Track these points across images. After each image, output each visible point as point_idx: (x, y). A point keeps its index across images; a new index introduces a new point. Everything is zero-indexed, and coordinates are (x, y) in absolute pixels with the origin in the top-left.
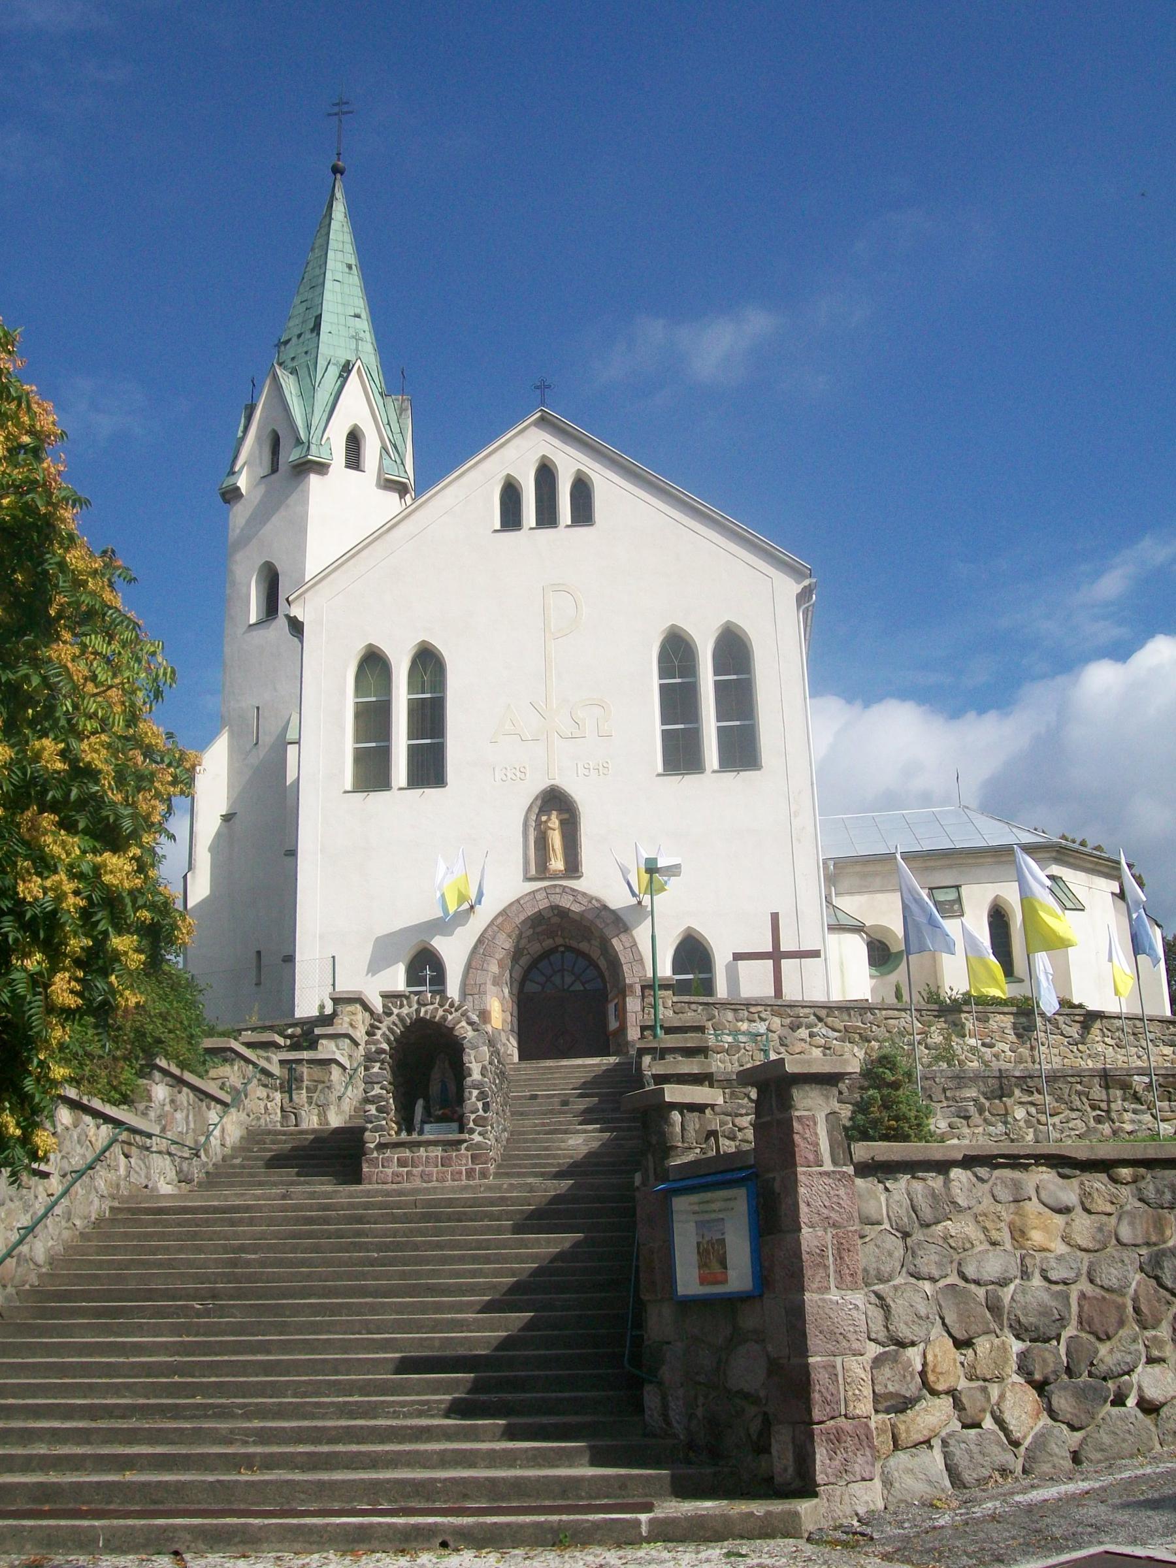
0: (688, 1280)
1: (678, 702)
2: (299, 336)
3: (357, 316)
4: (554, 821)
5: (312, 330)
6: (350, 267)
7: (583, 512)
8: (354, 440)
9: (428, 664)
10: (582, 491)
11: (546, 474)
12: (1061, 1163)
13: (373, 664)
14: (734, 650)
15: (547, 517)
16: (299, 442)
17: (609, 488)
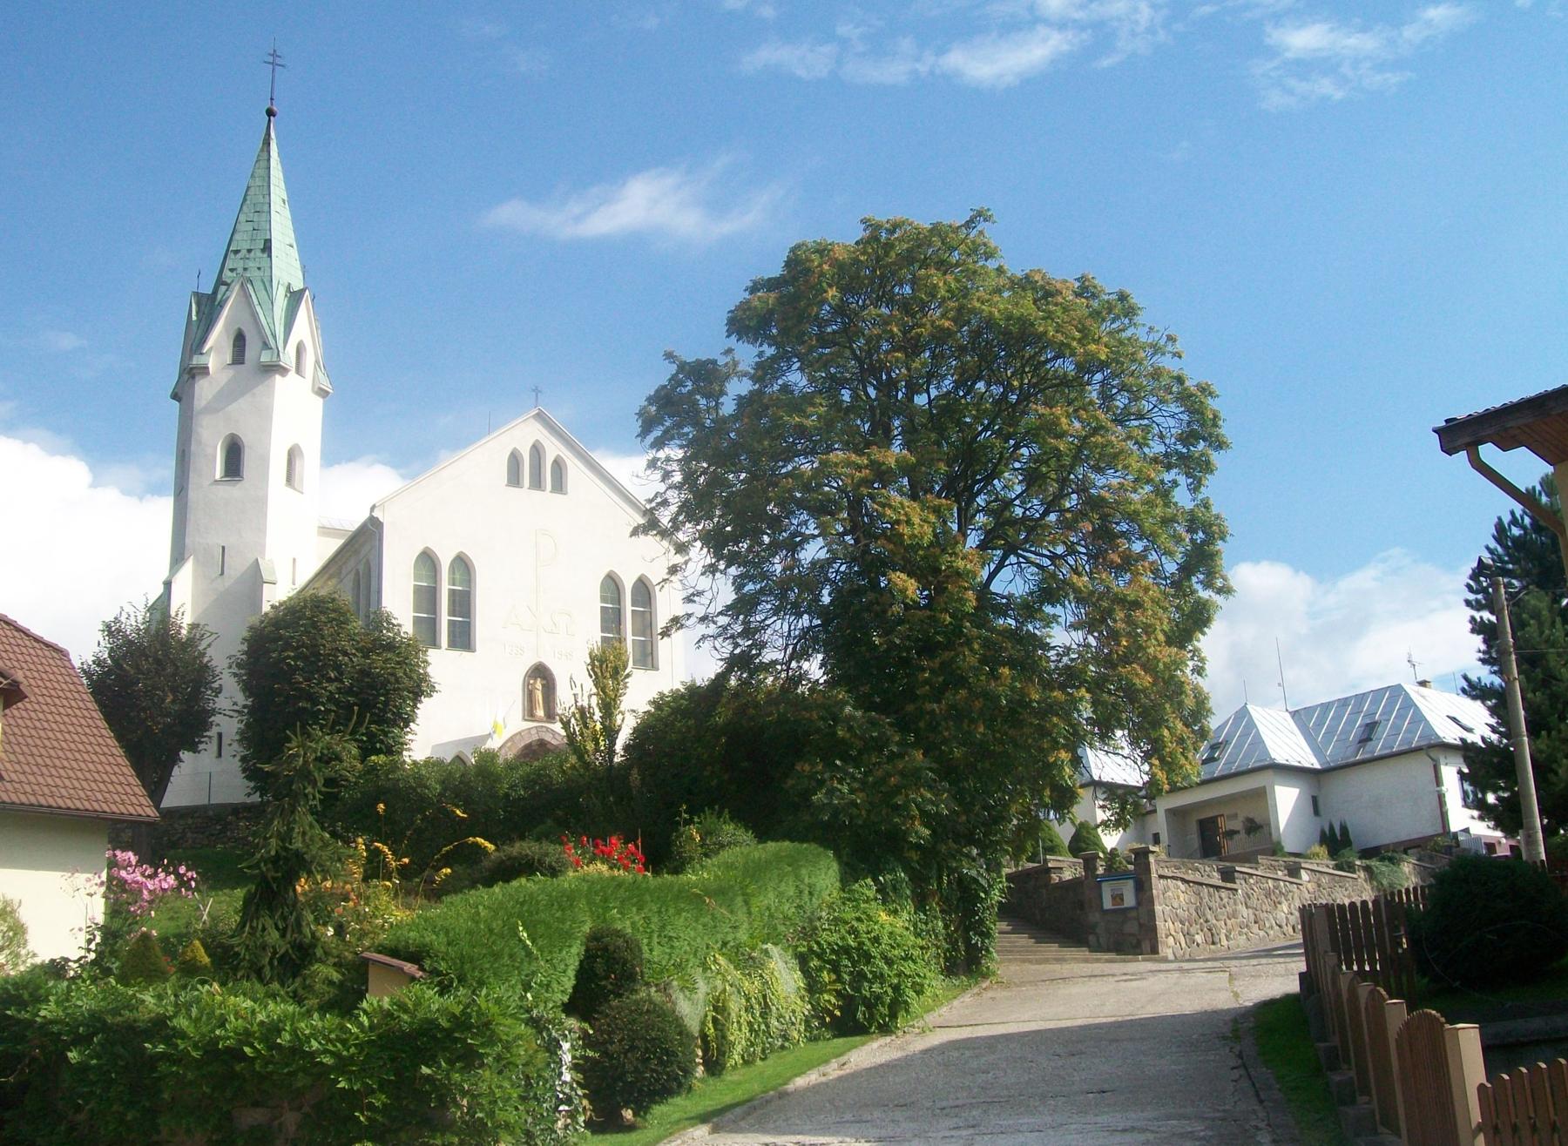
0: (1108, 904)
2: (249, 251)
4: (539, 685)
5: (263, 251)
7: (559, 486)
8: (300, 350)
9: (463, 565)
10: (558, 465)
11: (537, 450)
12: (1183, 880)
13: (427, 560)
15: (537, 484)
16: (266, 346)
17: (576, 471)
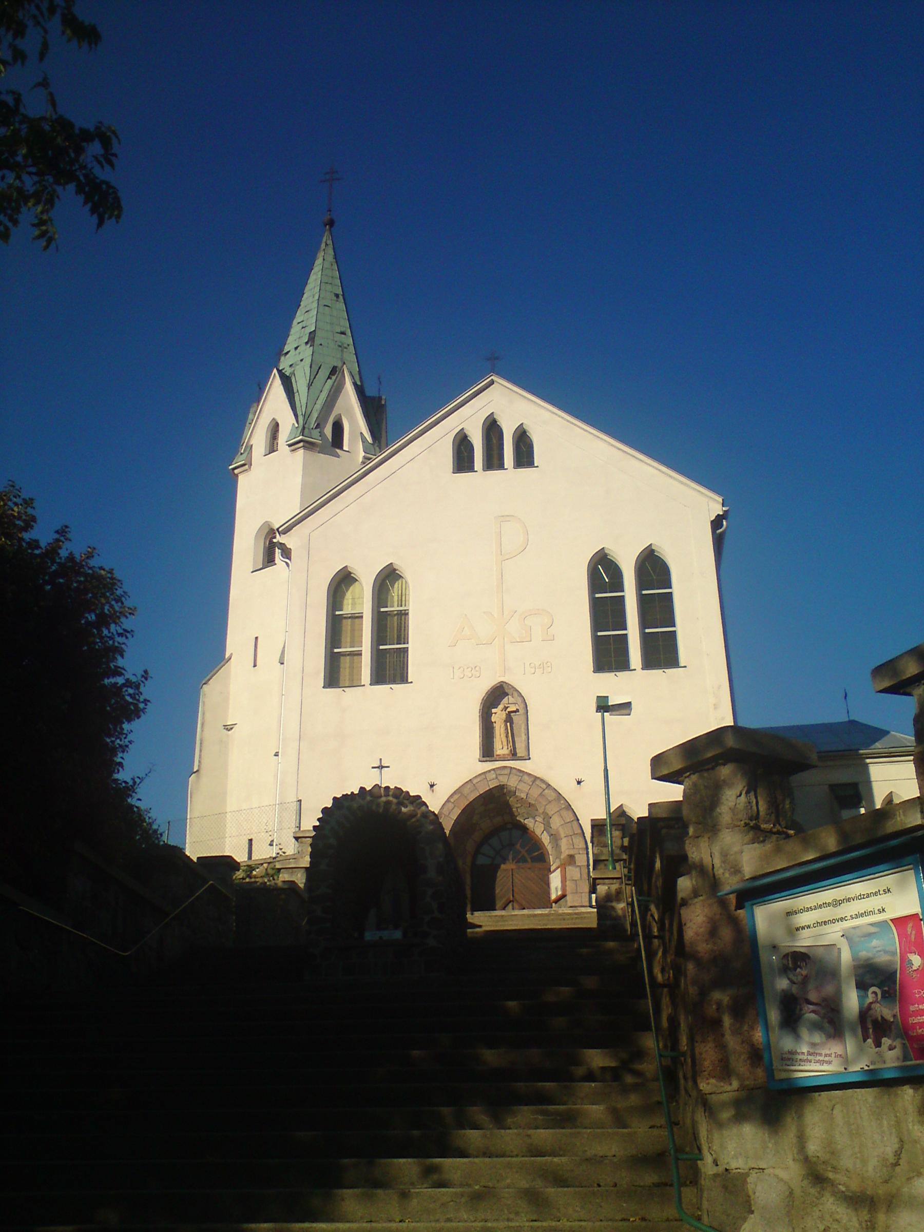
1: (606, 613)
2: (296, 348)
3: (343, 333)
6: (337, 296)
7: (525, 455)
11: (492, 428)
14: (653, 569)
15: (494, 461)
